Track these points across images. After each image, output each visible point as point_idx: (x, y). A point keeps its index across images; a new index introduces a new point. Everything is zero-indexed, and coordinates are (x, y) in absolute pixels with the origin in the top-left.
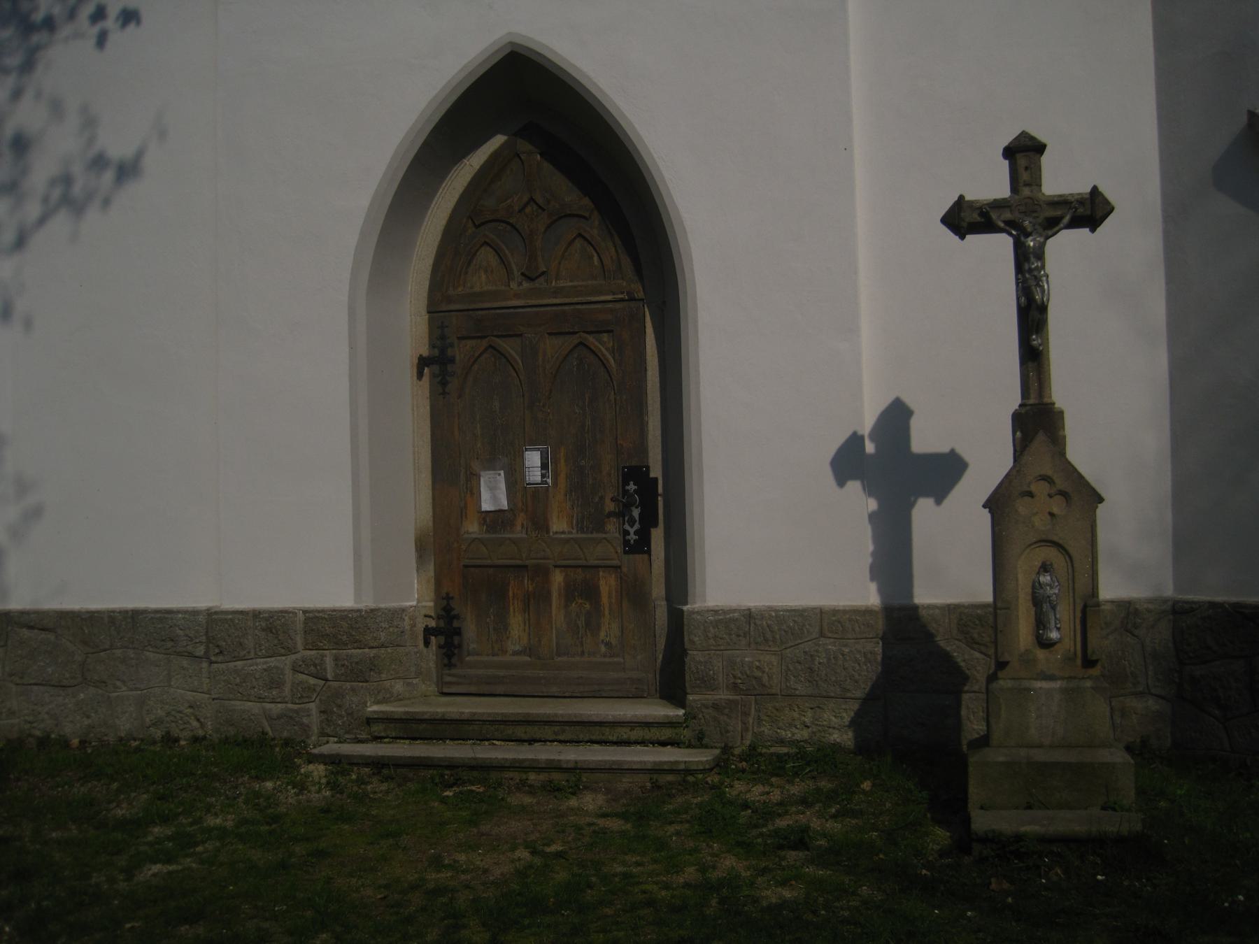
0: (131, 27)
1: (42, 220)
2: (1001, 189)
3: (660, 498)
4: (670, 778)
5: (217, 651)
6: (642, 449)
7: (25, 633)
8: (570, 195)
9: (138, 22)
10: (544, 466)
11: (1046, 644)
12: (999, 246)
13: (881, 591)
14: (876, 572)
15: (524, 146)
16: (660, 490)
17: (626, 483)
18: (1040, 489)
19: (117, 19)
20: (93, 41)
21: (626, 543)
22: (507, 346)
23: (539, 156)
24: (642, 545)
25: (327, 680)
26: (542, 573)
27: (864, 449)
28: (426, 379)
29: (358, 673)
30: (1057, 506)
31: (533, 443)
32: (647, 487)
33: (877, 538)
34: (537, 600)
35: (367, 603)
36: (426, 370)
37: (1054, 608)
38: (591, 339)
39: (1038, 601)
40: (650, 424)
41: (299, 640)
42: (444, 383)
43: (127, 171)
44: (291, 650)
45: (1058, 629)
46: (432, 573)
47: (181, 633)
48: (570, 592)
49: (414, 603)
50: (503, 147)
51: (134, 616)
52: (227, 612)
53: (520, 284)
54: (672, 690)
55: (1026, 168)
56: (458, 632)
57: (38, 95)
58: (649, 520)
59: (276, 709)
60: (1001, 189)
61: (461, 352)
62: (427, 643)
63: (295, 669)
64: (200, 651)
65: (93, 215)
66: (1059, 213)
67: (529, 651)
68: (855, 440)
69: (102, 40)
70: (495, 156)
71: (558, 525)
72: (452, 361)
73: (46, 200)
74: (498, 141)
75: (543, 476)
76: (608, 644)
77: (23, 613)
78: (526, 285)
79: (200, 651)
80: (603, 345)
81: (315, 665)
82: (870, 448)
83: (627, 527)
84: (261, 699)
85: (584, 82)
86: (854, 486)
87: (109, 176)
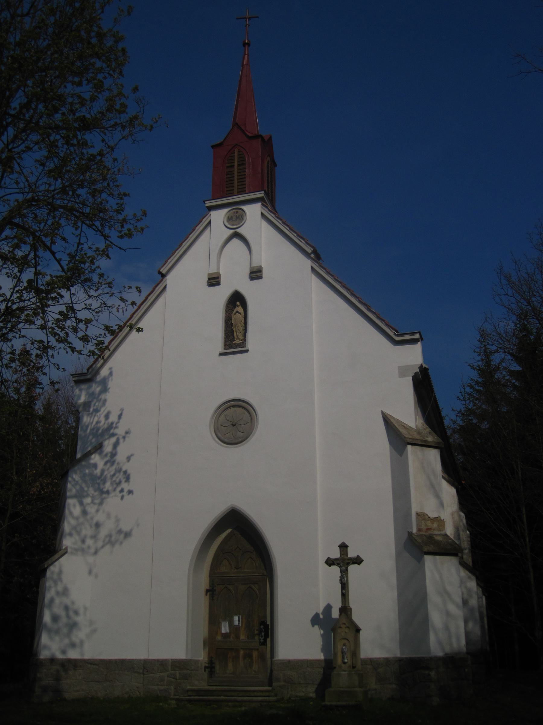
0: (131, 495)
1: (103, 547)
2: (338, 556)
3: (270, 630)
4: (265, 703)
5: (146, 671)
6: (265, 617)
7: (89, 665)
9: (133, 494)
10: (239, 621)
12: (336, 570)
13: (324, 655)
16: (270, 628)
17: (260, 626)
18: (343, 626)
19: (127, 493)
20: (120, 498)
21: (260, 642)
23: (240, 535)
24: (264, 643)
25: (176, 679)
27: (320, 617)
28: (208, 596)
30: (347, 630)
32: (266, 626)
33: (323, 641)
35: (189, 657)
36: (208, 593)
37: (346, 654)
38: (252, 586)
39: (343, 652)
40: (268, 610)
42: (213, 597)
43: (127, 535)
45: (347, 659)
46: (207, 650)
47: (136, 666)
49: (202, 659)
50: (231, 532)
51: (123, 661)
52: (150, 660)
53: (234, 570)
54: (270, 685)
55: (343, 551)
58: (266, 636)
59: (162, 688)
60: (338, 556)
62: (205, 671)
64: (141, 671)
65: (117, 546)
66: (349, 561)
68: (317, 615)
69: (122, 498)
71: (242, 637)
72: (215, 591)
73: (104, 541)
74: (229, 531)
75: (239, 623)
77: (89, 660)
78: (236, 570)
79: (141, 671)
81: (174, 675)
82: (321, 616)
83: (261, 638)
85: (251, 518)
86: (316, 627)
87: (122, 536)
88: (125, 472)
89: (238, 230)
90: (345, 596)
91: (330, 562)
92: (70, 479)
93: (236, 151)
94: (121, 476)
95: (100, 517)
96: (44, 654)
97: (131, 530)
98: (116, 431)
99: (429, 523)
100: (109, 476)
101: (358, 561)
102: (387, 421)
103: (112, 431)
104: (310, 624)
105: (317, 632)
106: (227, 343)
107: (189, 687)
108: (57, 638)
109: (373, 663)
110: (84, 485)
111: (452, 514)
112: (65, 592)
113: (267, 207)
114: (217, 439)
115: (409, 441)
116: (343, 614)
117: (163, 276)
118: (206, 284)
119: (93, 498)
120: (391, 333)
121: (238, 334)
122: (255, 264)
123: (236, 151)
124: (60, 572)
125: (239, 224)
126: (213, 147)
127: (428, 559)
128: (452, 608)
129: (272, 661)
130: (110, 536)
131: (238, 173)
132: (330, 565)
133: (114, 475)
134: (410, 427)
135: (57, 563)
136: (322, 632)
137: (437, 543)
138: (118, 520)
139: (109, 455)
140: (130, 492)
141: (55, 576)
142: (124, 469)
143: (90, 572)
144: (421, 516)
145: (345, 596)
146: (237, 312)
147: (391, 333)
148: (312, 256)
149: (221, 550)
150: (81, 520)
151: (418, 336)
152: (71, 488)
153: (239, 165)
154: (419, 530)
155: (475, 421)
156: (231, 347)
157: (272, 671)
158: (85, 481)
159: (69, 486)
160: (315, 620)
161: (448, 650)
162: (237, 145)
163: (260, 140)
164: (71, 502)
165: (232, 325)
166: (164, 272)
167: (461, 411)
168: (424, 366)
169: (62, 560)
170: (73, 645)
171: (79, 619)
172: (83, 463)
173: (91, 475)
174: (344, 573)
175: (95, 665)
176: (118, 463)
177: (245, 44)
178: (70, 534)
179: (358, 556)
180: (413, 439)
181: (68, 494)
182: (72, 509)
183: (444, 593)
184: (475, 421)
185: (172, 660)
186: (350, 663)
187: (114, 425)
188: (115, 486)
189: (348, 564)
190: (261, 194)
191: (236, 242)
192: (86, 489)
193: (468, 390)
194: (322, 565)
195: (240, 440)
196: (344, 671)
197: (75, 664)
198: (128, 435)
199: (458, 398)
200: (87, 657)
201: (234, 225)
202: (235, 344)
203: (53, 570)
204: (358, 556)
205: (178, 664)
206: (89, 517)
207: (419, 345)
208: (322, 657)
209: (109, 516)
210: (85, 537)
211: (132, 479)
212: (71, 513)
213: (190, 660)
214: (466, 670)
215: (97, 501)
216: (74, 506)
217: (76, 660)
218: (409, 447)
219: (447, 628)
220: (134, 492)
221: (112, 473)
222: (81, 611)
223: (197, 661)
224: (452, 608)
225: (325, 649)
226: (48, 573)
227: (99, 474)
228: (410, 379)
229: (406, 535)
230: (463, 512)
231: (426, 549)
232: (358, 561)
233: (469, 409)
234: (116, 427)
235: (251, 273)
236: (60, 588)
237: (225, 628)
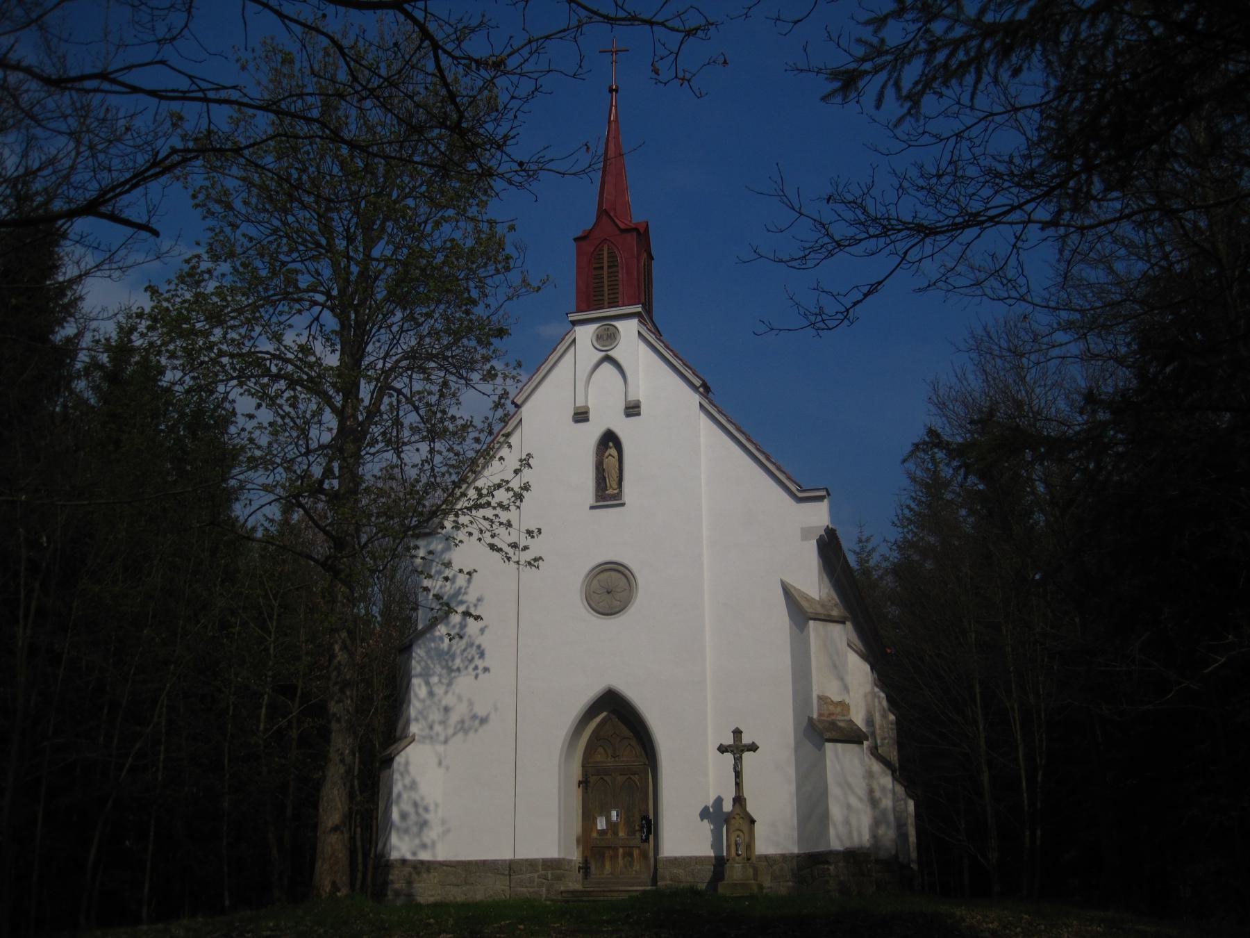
0: (487, 673)
1: (454, 734)
2: (731, 742)
6: (647, 810)
7: (445, 868)
8: (626, 731)
10: (617, 815)
11: (738, 855)
12: (729, 757)
14: (713, 846)
15: (613, 716)
18: (737, 817)
20: (473, 677)
22: (606, 778)
24: (647, 840)
26: (615, 849)
29: (559, 878)
30: (741, 821)
31: (614, 808)
32: (649, 822)
33: (713, 837)
34: (614, 858)
35: (562, 856)
39: (737, 844)
41: (540, 867)
43: (483, 721)
44: (538, 871)
48: (624, 855)
50: (605, 717)
51: (484, 862)
56: (589, 868)
57: (453, 693)
58: (649, 832)
59: (531, 890)
60: (731, 742)
61: (592, 779)
62: (579, 871)
63: (539, 877)
65: (471, 735)
67: (612, 873)
68: (706, 808)
69: (476, 676)
70: (604, 719)
71: (621, 834)
72: (589, 782)
73: (455, 728)
74: (604, 714)
76: (636, 871)
77: (444, 861)
80: (636, 778)
82: (711, 810)
84: (526, 887)
86: (706, 821)
87: (477, 722)
88: (479, 647)
89: (610, 353)
90: (738, 785)
91: (722, 749)
92: (414, 655)
93: (606, 246)
94: (473, 651)
95: (449, 700)
96: (395, 855)
97: (488, 715)
98: (465, 598)
99: (831, 708)
100: (458, 651)
101: (753, 748)
102: (787, 591)
103: (460, 598)
104: (699, 819)
105: (707, 827)
106: (600, 494)
107: (562, 888)
108: (407, 838)
109: (766, 858)
110: (429, 662)
111: (865, 696)
112: (413, 786)
113: (645, 325)
114: (592, 612)
115: (811, 616)
116: (737, 804)
117: (518, 406)
118: (571, 418)
119: (440, 676)
120: (793, 487)
121: (612, 481)
122: (631, 398)
123: (606, 246)
124: (407, 763)
125: (611, 345)
126: (576, 240)
127: (828, 746)
128: (853, 801)
129: (656, 860)
130: (463, 722)
131: (608, 277)
132: (722, 752)
133: (465, 650)
134: (813, 599)
135: (403, 753)
136: (712, 827)
137: (840, 728)
138: (471, 703)
139: (458, 626)
140: (486, 670)
141: (402, 768)
142: (477, 643)
143: (440, 763)
144: (823, 699)
145: (738, 785)
146: (610, 455)
147: (793, 487)
148: (701, 390)
149: (596, 736)
150: (428, 702)
151: (824, 493)
152: (416, 667)
153: (609, 267)
154: (820, 715)
155: (916, 557)
156: (604, 499)
157: (656, 869)
158: (431, 658)
159: (414, 662)
160: (705, 814)
161: (848, 844)
162: (606, 239)
163: (635, 234)
164: (416, 682)
165: (604, 470)
166: (519, 402)
167: (896, 543)
168: (830, 526)
169: (409, 749)
170: (424, 846)
171: (430, 817)
172: (428, 636)
173: (437, 649)
174: (738, 761)
175: (452, 867)
176: (469, 636)
177: (611, 91)
178: (417, 720)
179: (753, 743)
180: (816, 614)
181: (413, 672)
182: (416, 689)
183: (846, 786)
184: (916, 557)
185: (543, 859)
186: (744, 855)
187: (463, 590)
188: (467, 663)
189: (743, 751)
190: (638, 308)
191: (606, 366)
192: (432, 666)
193: (906, 511)
194: (712, 750)
195: (617, 610)
196: (738, 863)
197: (428, 866)
198: (480, 603)
199: (893, 523)
200: (440, 858)
201: (606, 346)
202: (608, 495)
203: (399, 760)
204: (753, 743)
205: (549, 864)
206: (436, 699)
207: (826, 502)
208: (712, 854)
209: (460, 698)
210: (433, 722)
211: (487, 652)
212: (416, 695)
213: (564, 859)
214: (869, 866)
215: (445, 681)
216: (420, 686)
217: (429, 862)
218: (811, 623)
219: (847, 822)
220: (491, 670)
221: (463, 648)
222: (432, 807)
223: (570, 861)
224: (853, 801)
225: (716, 843)
226: (395, 765)
227: (446, 649)
228: (814, 542)
229: (806, 721)
230: (884, 692)
231: (827, 735)
232: (753, 748)
233: (909, 541)
234: (466, 593)
235: (627, 408)
236: (407, 781)
237: (601, 824)
